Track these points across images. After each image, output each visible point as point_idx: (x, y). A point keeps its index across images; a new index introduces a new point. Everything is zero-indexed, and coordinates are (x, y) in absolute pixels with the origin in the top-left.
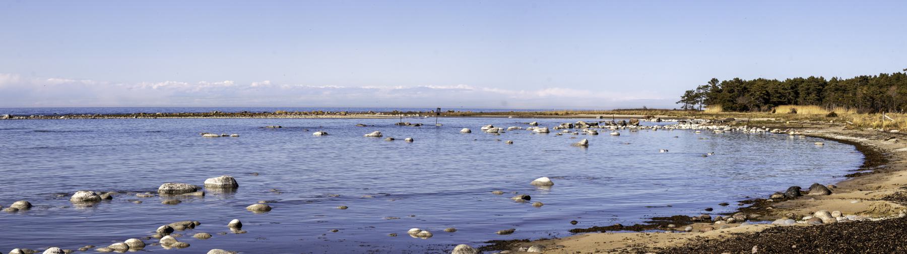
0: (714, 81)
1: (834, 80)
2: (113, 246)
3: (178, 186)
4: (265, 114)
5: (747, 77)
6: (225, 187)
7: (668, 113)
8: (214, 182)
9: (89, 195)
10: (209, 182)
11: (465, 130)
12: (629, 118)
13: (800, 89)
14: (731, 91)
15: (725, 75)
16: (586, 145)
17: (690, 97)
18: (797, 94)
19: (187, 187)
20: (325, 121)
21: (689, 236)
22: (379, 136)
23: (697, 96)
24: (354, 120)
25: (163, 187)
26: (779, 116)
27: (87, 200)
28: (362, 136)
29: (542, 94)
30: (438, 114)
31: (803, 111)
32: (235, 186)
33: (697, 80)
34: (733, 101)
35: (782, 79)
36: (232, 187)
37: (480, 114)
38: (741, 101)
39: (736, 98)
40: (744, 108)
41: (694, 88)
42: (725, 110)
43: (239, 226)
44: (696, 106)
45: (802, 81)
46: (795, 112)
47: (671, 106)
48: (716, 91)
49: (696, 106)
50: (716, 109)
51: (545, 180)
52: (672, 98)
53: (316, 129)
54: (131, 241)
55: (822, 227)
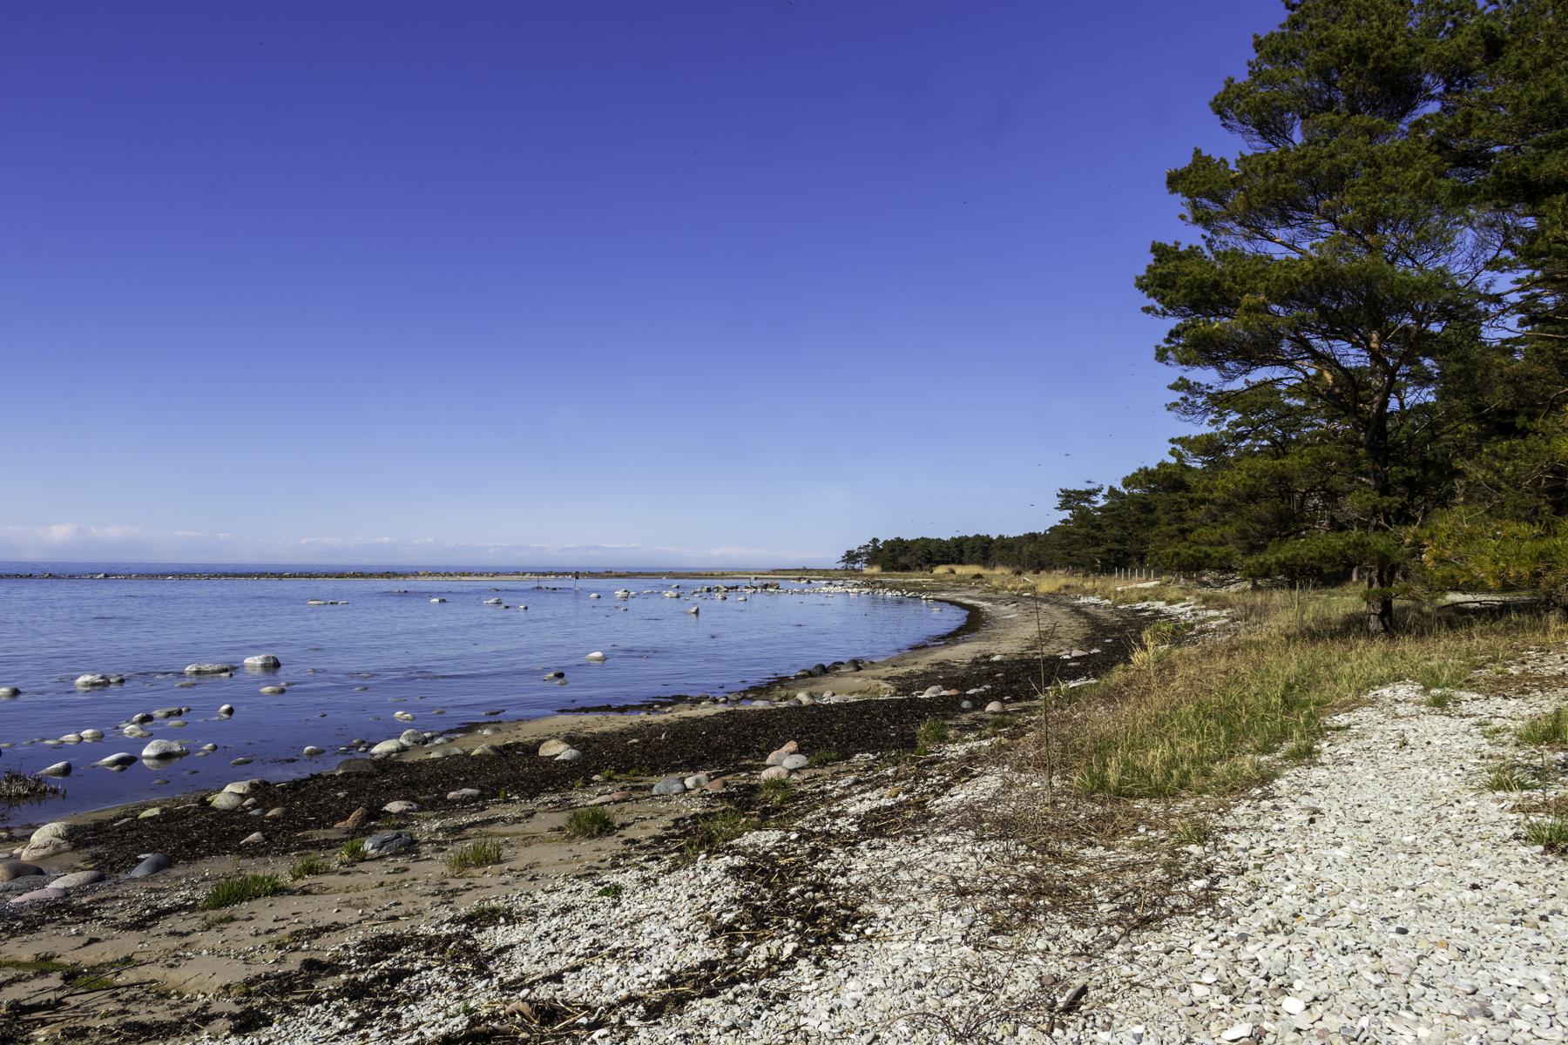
0: (875, 540)
1: (1001, 537)
2: (64, 738)
3: (207, 667)
4: (405, 575)
5: (909, 535)
6: (264, 666)
7: (828, 575)
8: (254, 661)
9: (97, 679)
10: (248, 661)
11: (594, 595)
12: (771, 580)
13: (965, 548)
14: (893, 551)
15: (886, 535)
16: (697, 612)
17: (851, 557)
18: (962, 552)
19: (216, 667)
20: (501, 583)
21: (668, 716)
22: (498, 603)
23: (858, 555)
24: (467, 583)
25: (190, 669)
26: (936, 577)
27: (93, 684)
28: (481, 604)
29: (717, 552)
30: (577, 575)
31: (960, 570)
32: (277, 665)
33: (858, 540)
34: (894, 560)
35: (946, 537)
36: (273, 666)
37: (608, 574)
38: (902, 560)
39: (898, 558)
40: (906, 568)
41: (855, 548)
42: (884, 569)
43: (230, 711)
44: (857, 566)
45: (967, 539)
46: (953, 572)
47: (832, 565)
48: (876, 549)
49: (857, 566)
50: (876, 570)
51: (598, 654)
52: (832, 557)
53: (431, 594)
54: (87, 733)
55: (800, 708)
